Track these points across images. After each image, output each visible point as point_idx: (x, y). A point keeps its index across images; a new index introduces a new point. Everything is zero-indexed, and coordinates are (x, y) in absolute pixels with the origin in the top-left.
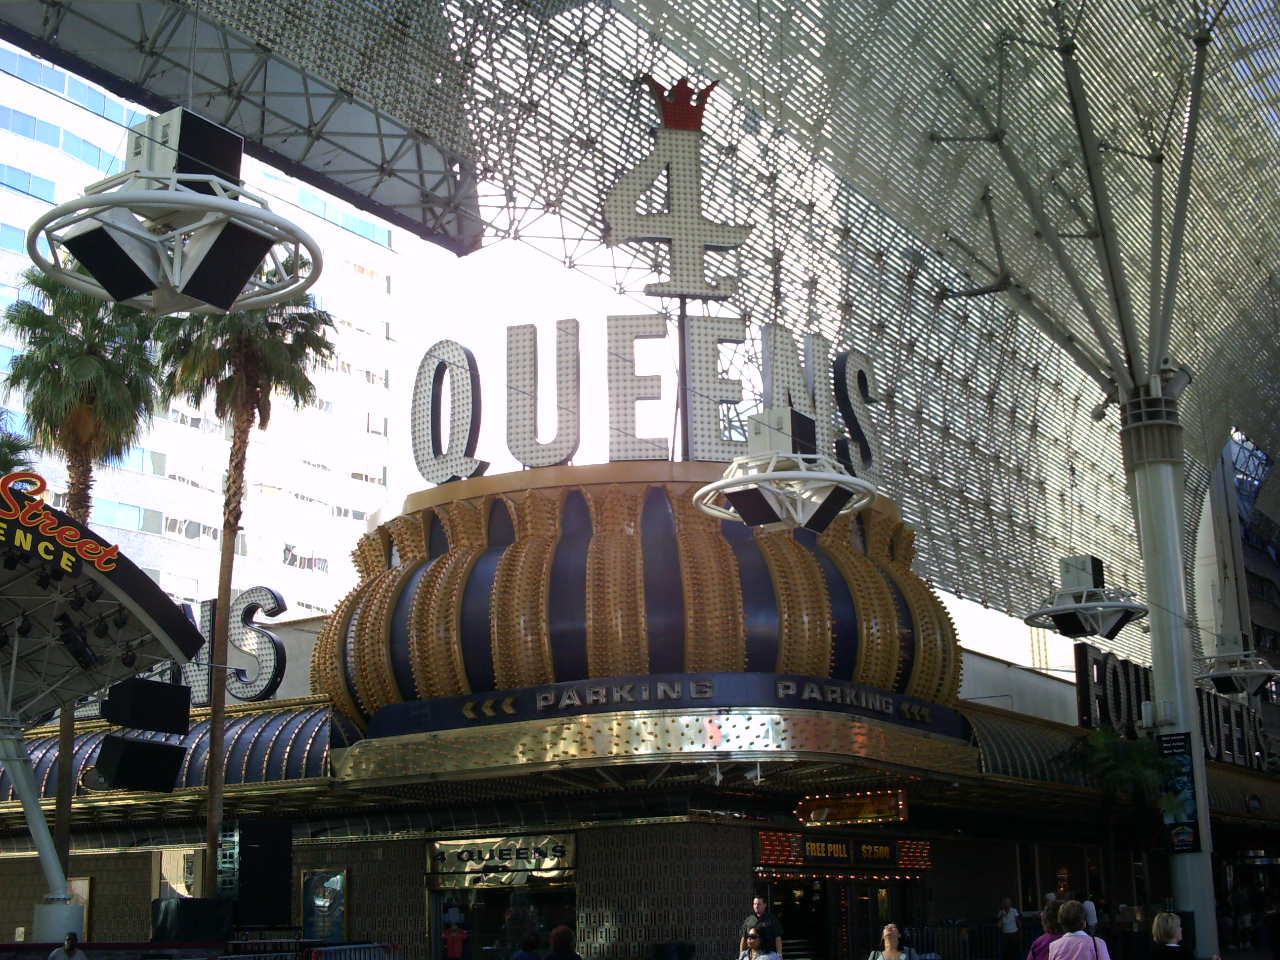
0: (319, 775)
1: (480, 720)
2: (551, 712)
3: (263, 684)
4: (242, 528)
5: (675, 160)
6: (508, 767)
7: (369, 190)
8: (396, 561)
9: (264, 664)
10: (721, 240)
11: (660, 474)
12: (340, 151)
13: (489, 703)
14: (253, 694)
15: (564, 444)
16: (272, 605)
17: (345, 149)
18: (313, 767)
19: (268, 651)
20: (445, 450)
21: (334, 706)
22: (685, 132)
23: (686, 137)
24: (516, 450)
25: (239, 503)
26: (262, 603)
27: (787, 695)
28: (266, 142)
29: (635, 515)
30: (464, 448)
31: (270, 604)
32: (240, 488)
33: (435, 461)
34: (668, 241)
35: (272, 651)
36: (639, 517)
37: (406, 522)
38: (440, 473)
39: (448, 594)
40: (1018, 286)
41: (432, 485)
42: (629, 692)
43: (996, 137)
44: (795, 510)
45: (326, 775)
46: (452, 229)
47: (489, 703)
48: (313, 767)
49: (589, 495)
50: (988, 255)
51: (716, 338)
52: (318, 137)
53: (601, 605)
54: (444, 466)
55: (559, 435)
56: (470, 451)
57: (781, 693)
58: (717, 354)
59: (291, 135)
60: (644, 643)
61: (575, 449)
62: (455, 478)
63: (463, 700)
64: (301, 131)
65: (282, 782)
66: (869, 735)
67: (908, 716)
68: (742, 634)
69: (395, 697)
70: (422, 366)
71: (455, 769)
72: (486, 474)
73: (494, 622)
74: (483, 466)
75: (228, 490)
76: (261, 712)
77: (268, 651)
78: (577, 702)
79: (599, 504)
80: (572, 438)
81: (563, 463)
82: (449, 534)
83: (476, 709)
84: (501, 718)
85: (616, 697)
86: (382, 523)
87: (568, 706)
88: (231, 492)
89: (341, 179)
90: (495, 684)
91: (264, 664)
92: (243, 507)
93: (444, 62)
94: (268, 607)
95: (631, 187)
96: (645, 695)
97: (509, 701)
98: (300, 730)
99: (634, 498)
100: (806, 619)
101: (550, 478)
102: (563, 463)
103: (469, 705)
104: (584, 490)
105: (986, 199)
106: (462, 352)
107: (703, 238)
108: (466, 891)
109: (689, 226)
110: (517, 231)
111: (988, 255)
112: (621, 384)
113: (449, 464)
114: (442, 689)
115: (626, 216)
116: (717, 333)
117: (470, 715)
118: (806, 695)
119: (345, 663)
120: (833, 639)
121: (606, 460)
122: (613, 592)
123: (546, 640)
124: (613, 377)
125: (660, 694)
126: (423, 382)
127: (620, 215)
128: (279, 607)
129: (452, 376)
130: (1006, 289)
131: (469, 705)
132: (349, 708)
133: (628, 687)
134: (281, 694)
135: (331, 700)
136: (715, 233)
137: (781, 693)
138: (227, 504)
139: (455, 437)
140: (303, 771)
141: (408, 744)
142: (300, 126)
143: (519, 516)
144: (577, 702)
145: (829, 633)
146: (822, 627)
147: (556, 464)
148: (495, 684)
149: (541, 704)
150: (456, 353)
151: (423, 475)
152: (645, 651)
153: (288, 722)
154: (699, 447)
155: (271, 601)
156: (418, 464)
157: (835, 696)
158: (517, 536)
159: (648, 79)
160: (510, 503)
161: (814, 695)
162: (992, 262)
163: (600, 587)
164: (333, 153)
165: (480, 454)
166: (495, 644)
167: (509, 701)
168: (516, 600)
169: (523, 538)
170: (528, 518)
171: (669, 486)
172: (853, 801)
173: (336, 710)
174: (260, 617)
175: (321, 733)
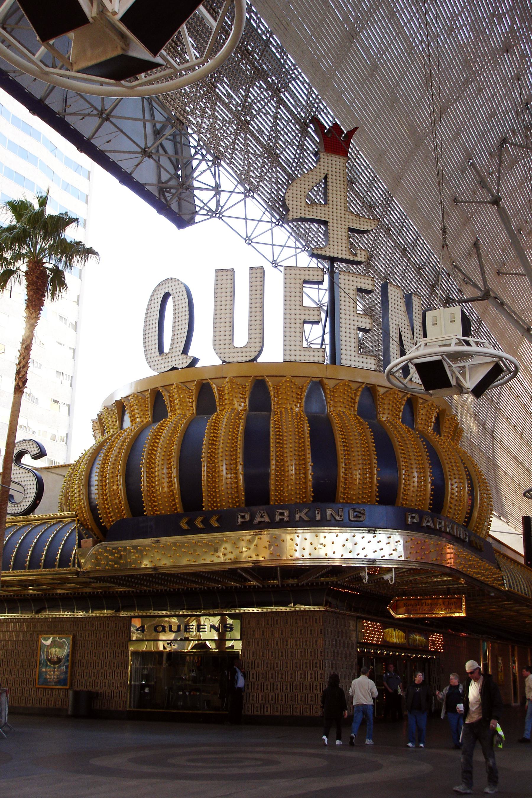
0: (69, 566)
1: (193, 530)
2: (244, 526)
3: (26, 504)
4: (26, 387)
5: (330, 173)
6: (213, 564)
7: (131, 169)
8: (127, 423)
9: (29, 491)
10: (359, 226)
11: (318, 373)
12: (119, 132)
13: (200, 519)
14: (19, 511)
15: (253, 349)
16: (37, 452)
17: (122, 131)
18: (65, 561)
19: (31, 483)
20: (166, 349)
21: (78, 520)
22: (337, 157)
23: (338, 160)
24: (219, 351)
25: (26, 373)
26: (29, 450)
27: (413, 523)
28: (68, 119)
29: (301, 399)
30: (182, 348)
31: (35, 451)
32: (27, 363)
33: (160, 358)
34: (325, 223)
35: (35, 482)
36: (303, 400)
37: (138, 396)
38: (162, 366)
39: (170, 442)
40: (496, 298)
41: (156, 373)
42: (306, 514)
43: (496, 201)
44: (465, 380)
45: (74, 566)
46: (174, 206)
47: (200, 519)
48: (65, 561)
49: (270, 383)
50: (477, 279)
52: (107, 119)
53: (281, 458)
54: (166, 361)
55: (249, 342)
56: (185, 351)
57: (410, 521)
59: (89, 115)
60: (310, 484)
61: (260, 352)
62: (174, 369)
63: (179, 517)
64: (95, 112)
65: (41, 570)
66: (456, 556)
67: (475, 545)
68: (375, 481)
69: (126, 514)
70: (155, 291)
71: (172, 564)
72: (197, 366)
73: (204, 464)
74: (195, 361)
75: (19, 364)
76: (25, 523)
77: (31, 483)
78: (267, 519)
79: (277, 389)
80: (258, 345)
81: (252, 361)
82: (168, 406)
83: (190, 523)
84: (209, 529)
85: (297, 517)
86: (118, 399)
87: (260, 523)
88: (22, 365)
89: (113, 157)
90: (203, 507)
91: (29, 491)
92: (28, 376)
93: (169, 99)
94: (34, 453)
95: (303, 186)
96: (318, 517)
97: (215, 518)
98: (55, 535)
99: (301, 389)
100: (416, 474)
101: (246, 370)
102: (255, 359)
103: (185, 520)
104: (267, 379)
105: (476, 245)
106: (182, 286)
107: (348, 224)
108: (161, 653)
109: (339, 215)
110: (221, 213)
111: (477, 279)
112: (293, 312)
113: (170, 360)
114: (163, 509)
115: (299, 204)
116: (356, 284)
117: (185, 527)
118: (424, 524)
119: (89, 493)
120: (432, 490)
121: (281, 361)
122: (290, 448)
123: (241, 477)
124: (217, 342)
125: (328, 517)
126: (153, 306)
127: (295, 203)
129: (174, 302)
130: (487, 299)
131: (185, 520)
132: (90, 523)
133: (305, 511)
135: (77, 516)
136: (355, 221)
137: (410, 521)
138: (18, 373)
139: (175, 342)
140: (57, 563)
141: (137, 546)
142: (96, 109)
143: (219, 395)
144: (267, 519)
145: (429, 485)
146: (425, 481)
147: (247, 362)
148: (203, 507)
149: (239, 520)
150: (178, 287)
151: (150, 367)
152: (310, 488)
153: (45, 530)
154: (343, 357)
155: (36, 449)
156: (147, 359)
157: (440, 526)
158: (218, 408)
159: (315, 121)
160: (214, 386)
161: (429, 524)
163: (280, 443)
164: (114, 135)
165: (192, 352)
166: (204, 478)
167: (215, 518)
168: (221, 450)
169: (222, 410)
170: (227, 397)
171: (326, 381)
172: (429, 601)
173: (82, 524)
174: (27, 460)
175: (71, 538)
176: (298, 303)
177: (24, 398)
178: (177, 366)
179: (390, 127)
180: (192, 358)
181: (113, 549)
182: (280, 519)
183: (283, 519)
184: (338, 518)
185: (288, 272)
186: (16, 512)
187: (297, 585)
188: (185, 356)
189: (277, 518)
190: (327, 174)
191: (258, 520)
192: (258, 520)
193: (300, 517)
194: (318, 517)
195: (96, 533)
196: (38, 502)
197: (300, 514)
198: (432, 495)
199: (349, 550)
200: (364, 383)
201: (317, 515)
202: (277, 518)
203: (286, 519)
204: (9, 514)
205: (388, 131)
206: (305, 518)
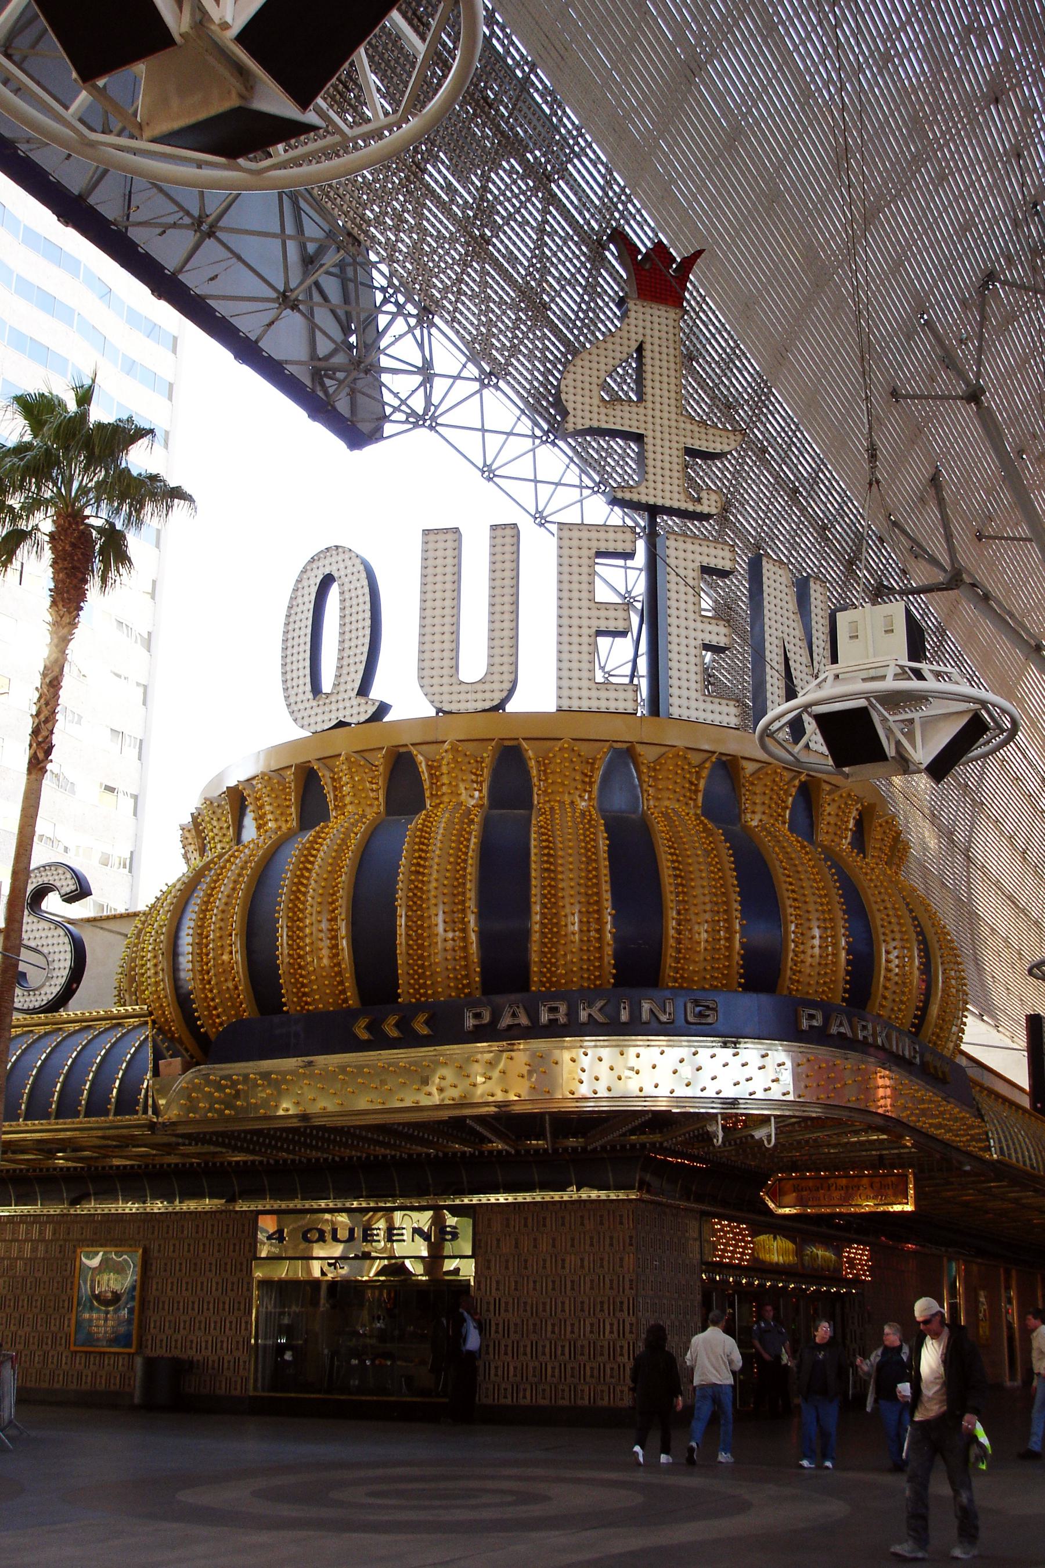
0: (136, 1113)
1: (380, 1042)
2: (480, 1034)
3: (52, 991)
4: (51, 761)
5: (648, 339)
6: (418, 1108)
7: (258, 332)
8: (250, 831)
9: (56, 965)
10: (705, 444)
11: (624, 733)
12: (234, 260)
13: (392, 1020)
14: (37, 1004)
15: (496, 686)
16: (73, 888)
17: (239, 258)
18: (127, 1103)
19: (62, 948)
20: (327, 686)
21: (154, 1022)
22: (663, 308)
23: (663, 313)
24: (430, 690)
25: (52, 732)
26: (58, 884)
27: (811, 1027)
28: (135, 234)
29: (591, 783)
30: (357, 685)
31: (69, 885)
32: (54, 713)
33: (315, 703)
34: (639, 438)
35: (68, 948)
36: (596, 787)
37: (271, 778)
38: (319, 719)
39: (335, 869)
40: (973, 585)
41: (306, 733)
42: (600, 1010)
43: (974, 396)
44: (914, 747)
45: (145, 1112)
47: (392, 1020)
48: (127, 1103)
49: (530, 753)
50: (937, 548)
51: (594, 630)
52: (211, 234)
53: (552, 901)
54: (327, 709)
55: (489, 673)
56: (364, 690)
57: (805, 1024)
58: (595, 649)
59: (174, 225)
60: (609, 951)
61: (511, 692)
62: (341, 724)
63: (352, 1015)
64: (187, 220)
65: (81, 1121)
66: (896, 1092)
67: (932, 1071)
68: (737, 945)
69: (247, 1010)
70: (304, 571)
71: (337, 1109)
72: (387, 719)
73: (401, 911)
74: (383, 709)
75: (38, 715)
76: (48, 1028)
77: (62, 948)
78: (524, 1020)
79: (544, 765)
80: (508, 677)
81: (495, 709)
82: (330, 797)
83: (374, 1027)
84: (410, 1039)
85: (583, 1016)
86: (232, 783)
87: (510, 1027)
88: (42, 717)
89: (222, 308)
90: (399, 996)
91: (56, 965)
92: (56, 739)
94: (66, 890)
95: (594, 365)
96: (624, 1016)
97: (422, 1018)
98: (108, 1052)
99: (592, 763)
100: (816, 932)
101: (484, 728)
102: (501, 706)
103: (363, 1022)
104: (525, 745)
105: (935, 481)
106: (358, 561)
107: (683, 439)
108: (316, 1284)
109: (666, 422)
110: (433, 418)
111: (937, 548)
112: (575, 612)
113: (334, 707)
114: (320, 1000)
115: (587, 400)
116: (699, 558)
117: (364, 1035)
118: (834, 1030)
119: (175, 968)
120: (848, 962)
121: (553, 709)
122: (569, 881)
123: (473, 937)
125: (645, 1016)
126: (300, 600)
127: (579, 398)
128: (81, 892)
129: (342, 593)
130: (957, 587)
131: (363, 1022)
132: (177, 1028)
133: (600, 1004)
134: (73, 1010)
135: (151, 1014)
136: (697, 435)
137: (805, 1024)
138: (36, 732)
139: (344, 671)
140: (112, 1107)
141: (270, 1073)
142: (188, 213)
143: (431, 775)
144: (524, 1020)
145: (843, 954)
146: (835, 945)
147: (484, 711)
148: (399, 996)
149: (470, 1022)
150: (349, 563)
151: (295, 720)
152: (609, 960)
153: (89, 1042)
154: (675, 701)
155: (71, 882)
156: (289, 705)
157: (865, 1033)
158: (428, 802)
159: (619, 237)
160: (420, 758)
161: (842, 1030)
162: (944, 559)
163: (550, 871)
164: (224, 264)
165: (377, 693)
166: (401, 939)
167: (422, 1018)
168: (434, 884)
169: (437, 806)
170: (445, 780)
171: (639, 749)
172: (844, 1182)
173: (161, 1030)
174: (52, 903)
175: (139, 1056)
176: (585, 595)
177: (47, 782)
178: (348, 720)
179: (766, 250)
180: (377, 704)
181: (222, 1078)
182: (550, 1020)
183: (557, 1020)
184: (664, 1018)
185: (566, 533)
186: (31, 1006)
187: (584, 1149)
188: (363, 700)
189: (544, 1017)
190: (642, 342)
191: (506, 1021)
192: (506, 1021)
193: (590, 1015)
194: (624, 1016)
195: (189, 1047)
196: (75, 986)
197: (588, 1011)
198: (848, 973)
199: (686, 1081)
200: (714, 752)
201: (623, 1012)
202: (544, 1017)
203: (562, 1019)
204: (18, 1010)
205: (762, 257)
206: (600, 1018)
